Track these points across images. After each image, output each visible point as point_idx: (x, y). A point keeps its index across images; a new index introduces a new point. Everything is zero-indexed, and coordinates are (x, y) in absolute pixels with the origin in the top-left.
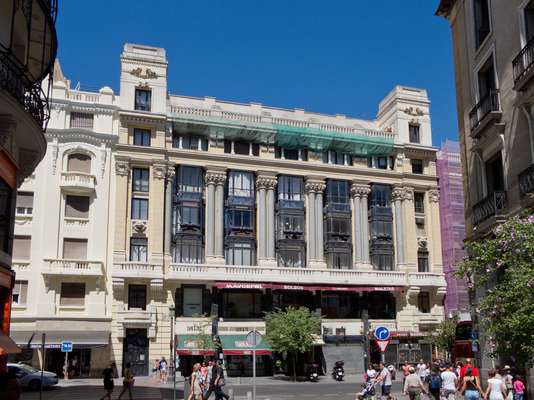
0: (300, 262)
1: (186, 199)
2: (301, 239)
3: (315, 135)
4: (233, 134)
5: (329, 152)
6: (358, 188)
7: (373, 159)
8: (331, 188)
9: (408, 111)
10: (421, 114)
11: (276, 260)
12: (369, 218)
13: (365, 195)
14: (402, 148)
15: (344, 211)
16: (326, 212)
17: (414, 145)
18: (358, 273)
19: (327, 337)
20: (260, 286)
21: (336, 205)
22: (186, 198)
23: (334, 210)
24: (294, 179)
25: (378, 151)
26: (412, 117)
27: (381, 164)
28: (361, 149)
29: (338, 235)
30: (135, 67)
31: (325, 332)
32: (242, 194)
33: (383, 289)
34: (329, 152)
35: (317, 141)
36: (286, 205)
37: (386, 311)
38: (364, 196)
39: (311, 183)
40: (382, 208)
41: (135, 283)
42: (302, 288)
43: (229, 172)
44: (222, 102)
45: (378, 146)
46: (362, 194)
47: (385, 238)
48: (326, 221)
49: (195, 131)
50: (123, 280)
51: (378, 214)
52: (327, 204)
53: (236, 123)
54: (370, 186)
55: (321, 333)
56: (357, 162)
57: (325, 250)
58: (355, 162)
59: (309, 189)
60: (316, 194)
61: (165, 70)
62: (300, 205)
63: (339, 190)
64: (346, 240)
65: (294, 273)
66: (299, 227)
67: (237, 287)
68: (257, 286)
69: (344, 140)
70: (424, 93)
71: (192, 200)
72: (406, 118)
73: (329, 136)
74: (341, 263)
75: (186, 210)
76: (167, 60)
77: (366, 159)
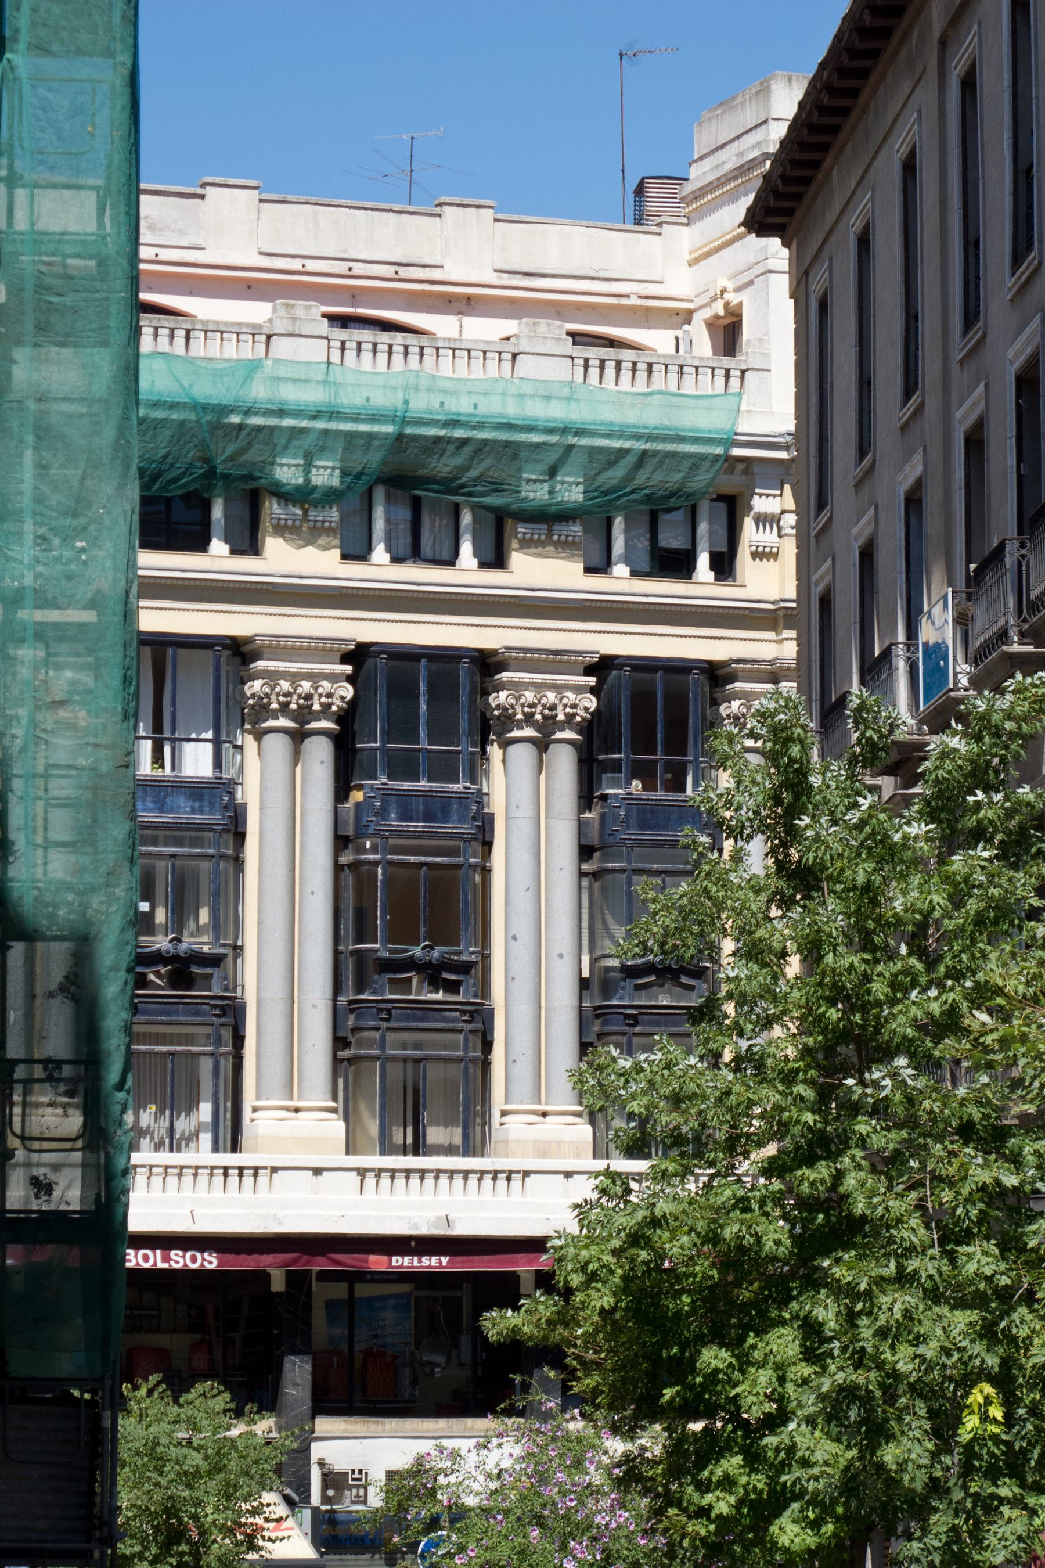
0: (205, 1111)
2: (217, 991)
3: (298, 414)
5: (379, 494)
6: (529, 696)
7: (618, 523)
8: (381, 696)
11: (334, 1111)
12: (585, 852)
13: (569, 734)
14: (780, 461)
15: (448, 827)
16: (350, 831)
18: (509, 1175)
19: (340, 1517)
21: (404, 797)
23: (394, 822)
24: (182, 652)
25: (650, 478)
27: (663, 544)
28: (552, 472)
29: (411, 964)
31: (330, 1493)
34: (379, 494)
35: (308, 442)
38: (559, 735)
39: (271, 677)
40: (659, 804)
42: (210, 1261)
45: (644, 452)
46: (548, 725)
47: (668, 969)
48: (349, 878)
51: (633, 834)
52: (360, 787)
54: (592, 680)
55: (307, 1499)
56: (526, 544)
57: (339, 1042)
58: (515, 544)
59: (262, 710)
60: (298, 737)
62: (212, 805)
63: (423, 707)
64: (453, 987)
65: (172, 1180)
66: (204, 916)
69: (459, 433)
74: (425, 1116)
77: (576, 529)
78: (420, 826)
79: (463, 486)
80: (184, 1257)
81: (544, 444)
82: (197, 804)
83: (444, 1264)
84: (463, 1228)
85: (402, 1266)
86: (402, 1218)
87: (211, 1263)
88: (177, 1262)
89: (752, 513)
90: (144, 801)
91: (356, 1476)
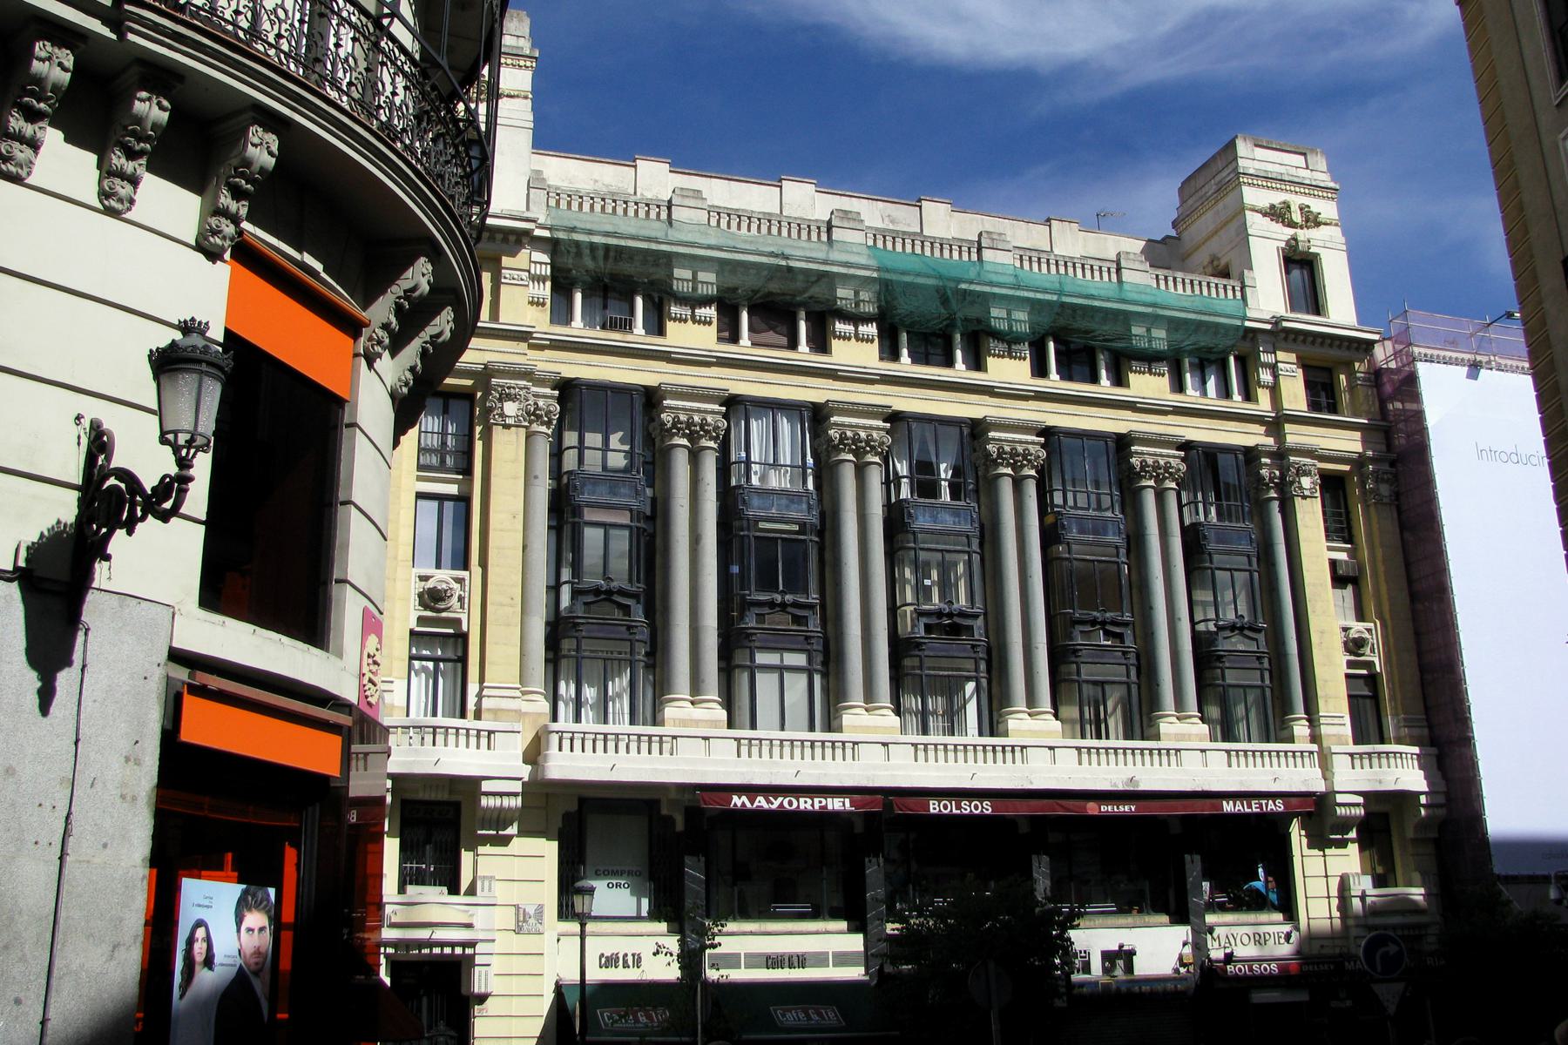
1: (593, 498)
4: (748, 282)
9: (1278, 214)
10: (1312, 220)
17: (1304, 322)
20: (847, 801)
22: (593, 493)
25: (1204, 340)
26: (1291, 231)
30: (1276, 198)
32: (776, 481)
33: (1250, 806)
36: (921, 518)
37: (1259, 885)
41: (423, 795)
42: (986, 808)
43: (734, 404)
44: (711, 177)
49: (627, 268)
50: (1360, 800)
53: (754, 246)
54: (1182, 454)
61: (528, 75)
67: (766, 806)
68: (835, 804)
70: (1320, 162)
71: (615, 500)
72: (1274, 236)
73: (1045, 291)
75: (1222, 576)
76: (533, 46)
78: (1091, 537)
79: (1095, 337)
80: (970, 806)
81: (846, 275)
82: (957, 520)
83: (1133, 810)
84: (1144, 786)
85: (1107, 811)
86: (1106, 779)
87: (987, 810)
88: (966, 810)
89: (614, 267)
90: (924, 516)
91: (1083, 954)
